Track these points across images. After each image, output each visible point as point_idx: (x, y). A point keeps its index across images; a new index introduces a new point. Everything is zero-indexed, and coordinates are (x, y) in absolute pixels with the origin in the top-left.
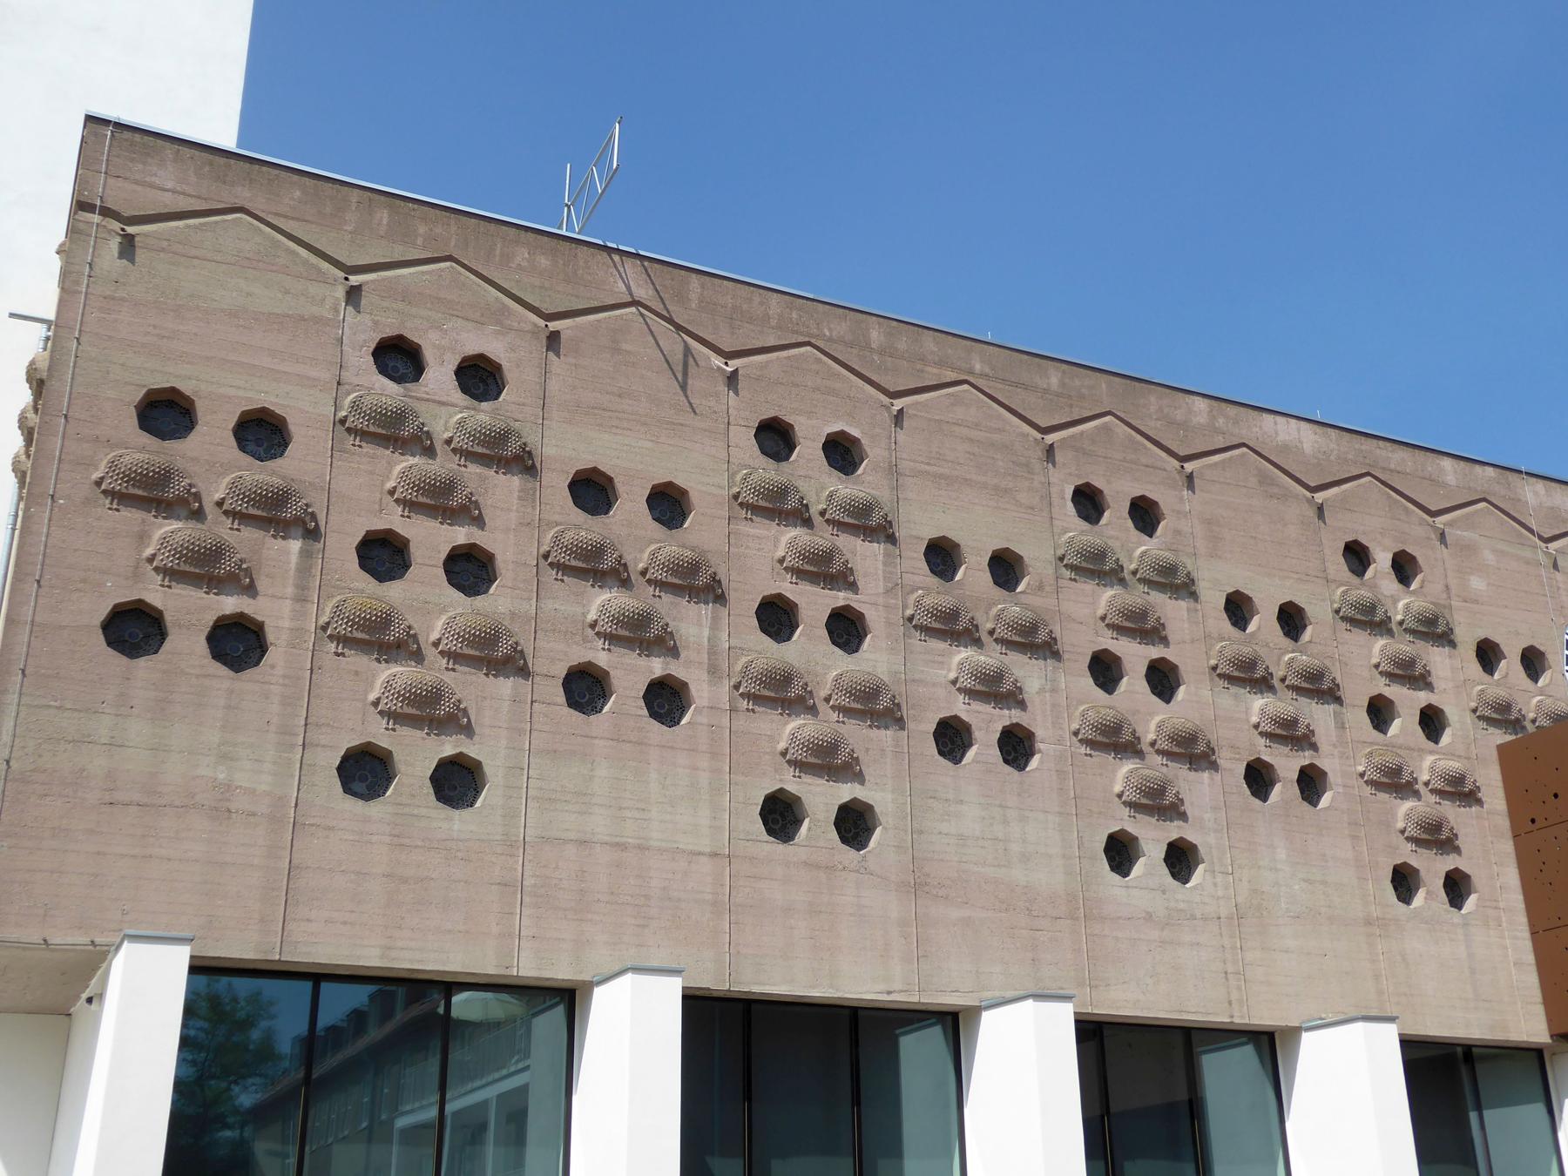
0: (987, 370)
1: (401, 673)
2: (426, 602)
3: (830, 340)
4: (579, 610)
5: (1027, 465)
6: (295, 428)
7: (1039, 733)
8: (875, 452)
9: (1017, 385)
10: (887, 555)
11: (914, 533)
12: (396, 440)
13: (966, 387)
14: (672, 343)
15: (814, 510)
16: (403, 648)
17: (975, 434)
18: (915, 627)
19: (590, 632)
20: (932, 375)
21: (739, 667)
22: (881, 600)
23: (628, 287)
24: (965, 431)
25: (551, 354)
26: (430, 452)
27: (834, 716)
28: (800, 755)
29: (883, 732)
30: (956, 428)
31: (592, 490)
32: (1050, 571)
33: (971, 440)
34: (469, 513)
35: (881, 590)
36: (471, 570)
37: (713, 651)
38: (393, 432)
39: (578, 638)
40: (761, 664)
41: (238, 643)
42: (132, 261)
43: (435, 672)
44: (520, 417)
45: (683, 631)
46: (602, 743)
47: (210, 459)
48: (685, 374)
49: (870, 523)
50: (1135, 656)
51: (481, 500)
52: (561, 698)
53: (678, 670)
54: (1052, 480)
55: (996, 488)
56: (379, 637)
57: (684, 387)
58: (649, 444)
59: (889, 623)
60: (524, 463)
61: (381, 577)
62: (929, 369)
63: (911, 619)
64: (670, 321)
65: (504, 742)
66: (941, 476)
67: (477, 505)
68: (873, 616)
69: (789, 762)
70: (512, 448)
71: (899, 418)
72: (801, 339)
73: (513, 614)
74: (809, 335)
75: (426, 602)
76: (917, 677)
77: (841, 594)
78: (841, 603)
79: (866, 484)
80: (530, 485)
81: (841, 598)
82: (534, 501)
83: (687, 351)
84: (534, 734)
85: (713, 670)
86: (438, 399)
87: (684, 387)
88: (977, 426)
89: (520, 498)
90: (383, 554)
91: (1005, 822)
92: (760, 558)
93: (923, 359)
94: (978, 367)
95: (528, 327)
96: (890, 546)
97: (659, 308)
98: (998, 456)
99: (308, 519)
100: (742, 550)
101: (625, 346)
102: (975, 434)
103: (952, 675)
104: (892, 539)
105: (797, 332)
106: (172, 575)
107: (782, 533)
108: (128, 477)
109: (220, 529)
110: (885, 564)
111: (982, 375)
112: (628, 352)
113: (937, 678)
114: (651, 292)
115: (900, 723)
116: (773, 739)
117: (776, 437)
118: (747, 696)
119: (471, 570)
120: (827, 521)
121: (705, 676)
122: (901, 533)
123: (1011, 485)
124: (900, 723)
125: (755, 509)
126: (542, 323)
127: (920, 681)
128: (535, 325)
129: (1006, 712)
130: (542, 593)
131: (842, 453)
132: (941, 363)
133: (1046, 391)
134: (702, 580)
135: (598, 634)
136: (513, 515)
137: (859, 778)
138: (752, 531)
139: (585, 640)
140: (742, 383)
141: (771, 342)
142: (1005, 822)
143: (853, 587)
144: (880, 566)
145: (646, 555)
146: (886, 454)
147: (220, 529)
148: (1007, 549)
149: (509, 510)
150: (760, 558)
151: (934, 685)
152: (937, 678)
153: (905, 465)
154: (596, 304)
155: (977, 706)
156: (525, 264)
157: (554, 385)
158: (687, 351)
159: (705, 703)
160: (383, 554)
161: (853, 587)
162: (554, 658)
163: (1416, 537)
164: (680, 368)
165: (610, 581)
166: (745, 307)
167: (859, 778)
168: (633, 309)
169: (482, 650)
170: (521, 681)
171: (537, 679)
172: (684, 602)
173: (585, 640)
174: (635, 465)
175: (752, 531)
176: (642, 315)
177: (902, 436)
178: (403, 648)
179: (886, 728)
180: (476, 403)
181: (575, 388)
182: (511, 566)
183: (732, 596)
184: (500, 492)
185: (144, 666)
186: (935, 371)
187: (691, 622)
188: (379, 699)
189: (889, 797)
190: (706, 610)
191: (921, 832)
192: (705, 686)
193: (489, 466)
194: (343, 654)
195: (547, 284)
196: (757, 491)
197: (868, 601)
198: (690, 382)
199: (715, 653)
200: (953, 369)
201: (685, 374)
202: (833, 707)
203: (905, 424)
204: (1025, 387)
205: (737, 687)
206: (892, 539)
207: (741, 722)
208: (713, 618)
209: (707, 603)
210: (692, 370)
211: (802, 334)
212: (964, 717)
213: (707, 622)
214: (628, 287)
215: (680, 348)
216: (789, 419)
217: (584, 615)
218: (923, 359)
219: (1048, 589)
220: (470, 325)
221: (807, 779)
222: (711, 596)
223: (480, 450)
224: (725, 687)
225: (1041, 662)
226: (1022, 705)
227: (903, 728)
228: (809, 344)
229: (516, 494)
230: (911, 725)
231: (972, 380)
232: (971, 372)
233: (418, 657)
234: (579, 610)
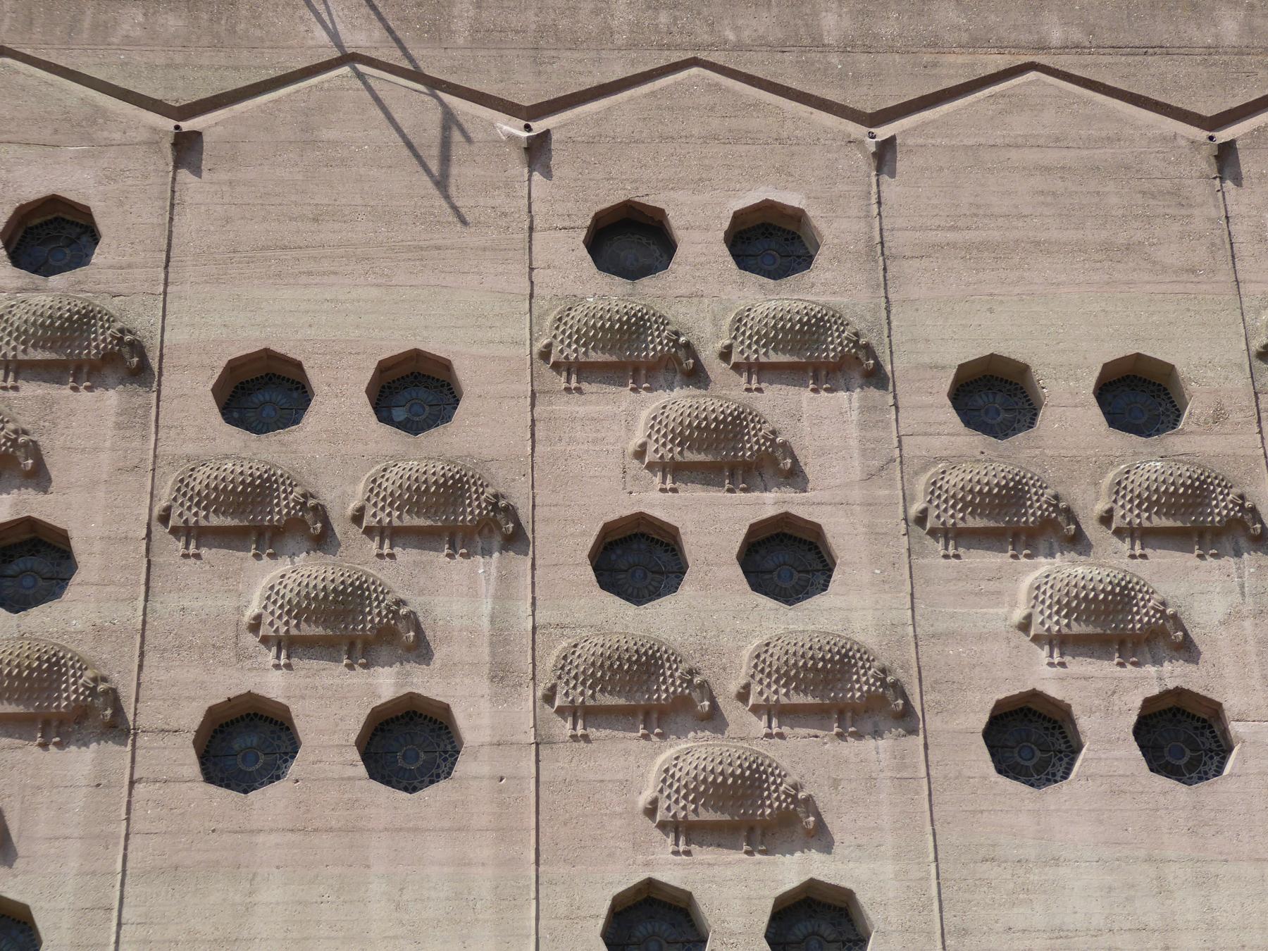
0: (1077, 35)
1: (692, 752)
2: (717, 620)
3: (739, 47)
4: (229, 603)
5: (1175, 193)
6: (464, 373)
7: (1232, 702)
8: (835, 229)
9: (1145, 50)
10: (865, 409)
11: (926, 359)
12: (636, 369)
13: (1032, 75)
14: (418, 111)
15: (709, 355)
16: (689, 708)
17: (1052, 156)
18: (933, 533)
19: (251, 640)
20: (955, 69)
21: (549, 662)
22: (856, 494)
23: (334, 36)
24: (1032, 156)
25: (184, 174)
26: (696, 376)
27: (761, 726)
28: (683, 810)
29: (869, 744)
30: (1014, 154)
31: (994, 394)
32: (1241, 381)
33: (1047, 169)
34: (776, 465)
35: (857, 473)
36: (787, 559)
37: (500, 637)
38: (630, 355)
39: (228, 654)
40: (592, 648)
41: (409, 745)
42: (1238, 180)
43: (746, 737)
44: (121, 288)
45: (439, 611)
46: (274, 839)
47: (340, 450)
48: (445, 159)
49: (833, 358)
50: (714, 522)
51: (43, 442)
52: (191, 766)
53: (426, 683)
54: (1233, 210)
55: (1106, 247)
56: (636, 693)
57: (442, 183)
58: (375, 292)
59: (875, 534)
60: (860, 367)
61: (790, 594)
62: (951, 58)
63: (921, 519)
64: (415, 75)
65: (73, 864)
66: (983, 246)
67: (787, 448)
68: (842, 533)
69: (663, 826)
70: (99, 341)
71: (885, 155)
72: (676, 57)
73: (98, 630)
74: (698, 47)
75: (717, 620)
76: (941, 626)
77: (770, 496)
78: (769, 512)
79: (826, 287)
80: (138, 401)
81: (768, 503)
82: (145, 426)
83: (449, 120)
84: (135, 841)
85: (500, 674)
86: (705, 293)
87: (442, 183)
88: (1058, 141)
89: (118, 426)
90: (636, 558)
91: (1162, 889)
92: (600, 459)
93: (935, 44)
94: (1056, 35)
95: (144, 135)
96: (873, 393)
97: (393, 56)
98: (1111, 187)
99: (309, 517)
100: (559, 447)
101: (326, 134)
102: (1052, 156)
103: (1018, 615)
104: (877, 377)
105: (669, 47)
106: (291, 646)
107: (643, 404)
108: (1150, 502)
109: (359, 558)
110: (863, 426)
111: (1065, 48)
112: (334, 143)
113: (985, 627)
114: (378, 33)
115: (907, 719)
116: (626, 786)
117: (630, 237)
118: (572, 712)
119: (787, 559)
120: (737, 367)
121: (484, 687)
122: (899, 364)
123: (1139, 236)
124: (907, 719)
125: (582, 371)
126: (1201, 135)
127: (950, 635)
128: (154, 130)
129: (1151, 670)
130: (156, 584)
131: (770, 241)
132: (975, 44)
133: (1212, 50)
134: (470, 513)
135: (265, 640)
136: (105, 457)
137: (820, 837)
138: (582, 411)
139: (241, 655)
140: (559, 154)
141: (618, 71)
142: (1162, 889)
143: (794, 477)
144: (854, 431)
145: (361, 487)
146: (861, 226)
147: (359, 558)
148: (1138, 357)
149: (96, 449)
150: (600, 459)
151: (980, 638)
152: (985, 627)
153: (895, 242)
154: (272, 73)
155: (1080, 666)
156: (138, 32)
157: (187, 223)
158: (449, 120)
159: (485, 736)
160: (636, 558)
161: (794, 477)
162: (175, 701)
163: (811, 173)
164: (435, 151)
165: (291, 544)
166: (563, 23)
167: (820, 837)
168: (345, 70)
169: (27, 702)
170: (111, 747)
171: (143, 740)
172: (441, 558)
173: (241, 655)
174: (339, 331)
175: (582, 411)
176: (360, 76)
177: (891, 188)
178: (689, 708)
179: (877, 734)
180: (38, 279)
181: (228, 220)
182: (98, 546)
183: (542, 534)
184: (819, 421)
185: (270, 800)
186: (961, 59)
187: (456, 594)
188: (654, 802)
189: (889, 869)
190: (484, 569)
191: (965, 932)
192: (485, 705)
193: (60, 381)
194: (781, 736)
195: (179, 59)
196: (584, 338)
197: (828, 499)
198: (454, 170)
199: (506, 642)
200: (1001, 49)
201: (445, 159)
202: (756, 710)
203: (901, 165)
204: (1164, 50)
205: (549, 698)
206: (877, 377)
207: (564, 763)
208: (502, 579)
209: (487, 552)
210: (459, 149)
211: (678, 47)
212: (1053, 690)
213: (487, 589)
214: (334, 36)
215: (434, 117)
216: (654, 200)
217: (239, 610)
218: (935, 44)
219: (1237, 417)
220: (32, 152)
221: (704, 854)
222: (497, 540)
223: (38, 355)
224: (524, 707)
225: (1229, 562)
226: (1187, 649)
227: (913, 731)
228: (694, 62)
229: (111, 421)
230: (933, 723)
231: (702, 55)
232: (1043, 48)
233: (713, 719)
234: (229, 603)
